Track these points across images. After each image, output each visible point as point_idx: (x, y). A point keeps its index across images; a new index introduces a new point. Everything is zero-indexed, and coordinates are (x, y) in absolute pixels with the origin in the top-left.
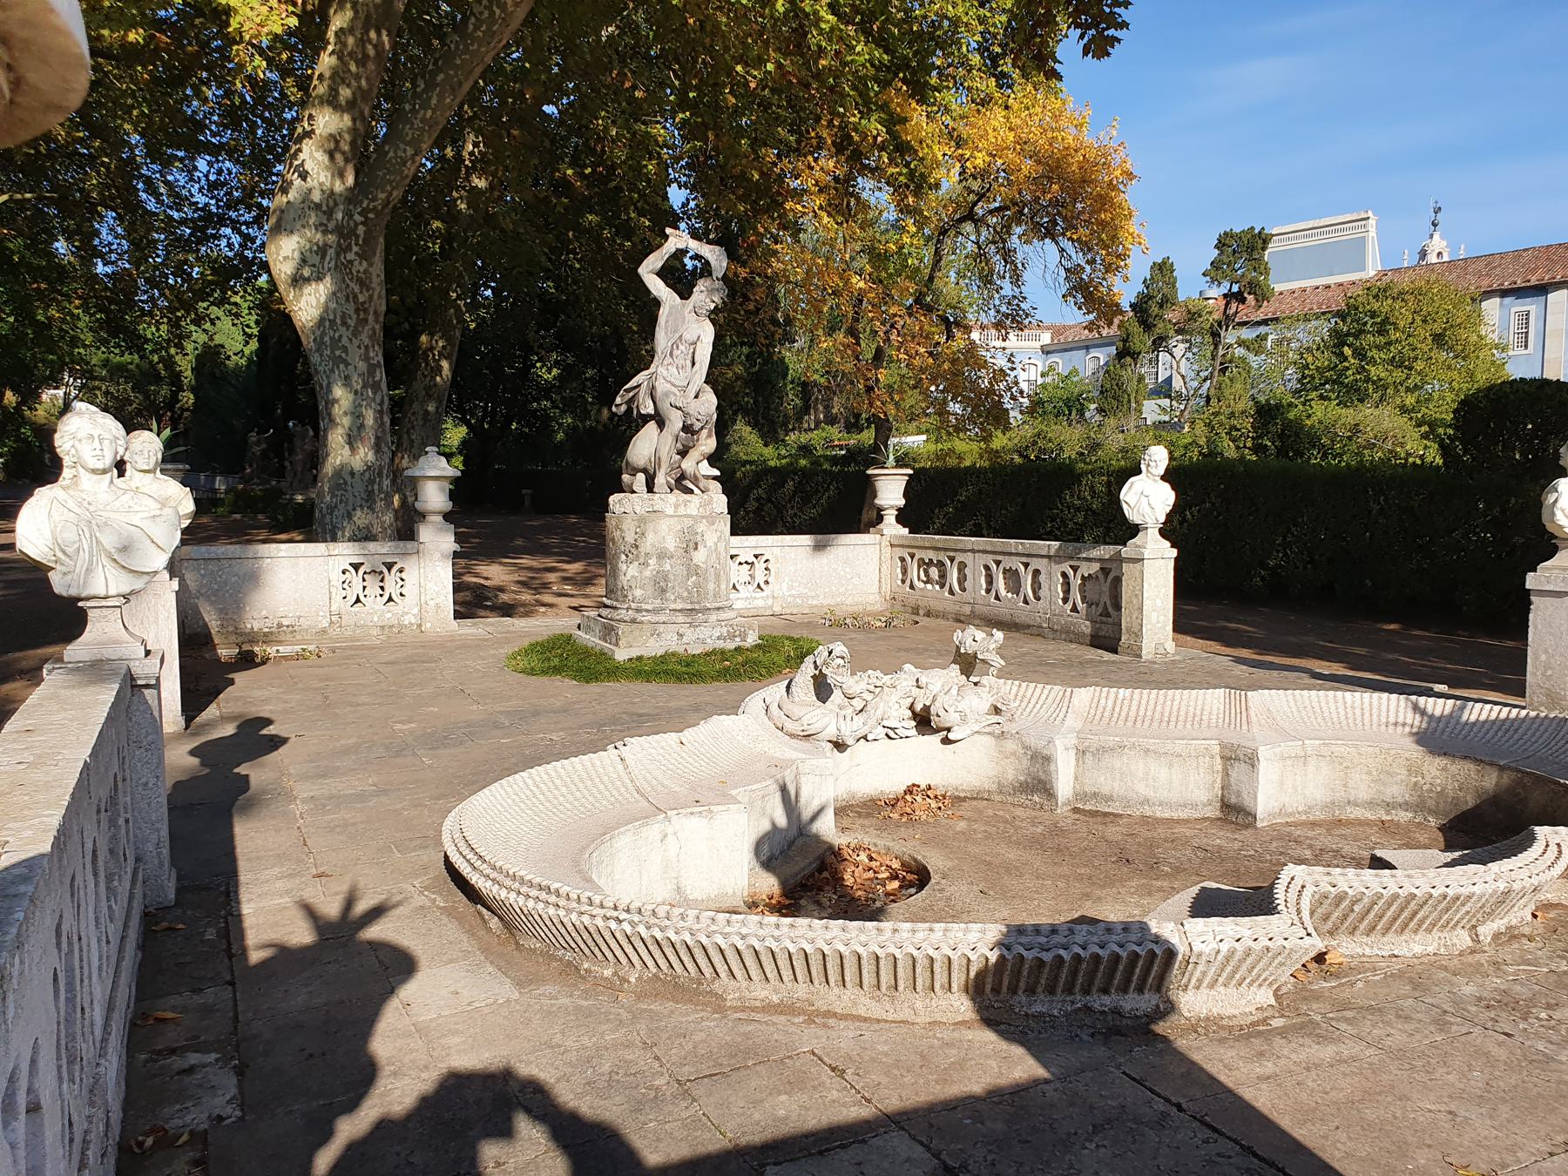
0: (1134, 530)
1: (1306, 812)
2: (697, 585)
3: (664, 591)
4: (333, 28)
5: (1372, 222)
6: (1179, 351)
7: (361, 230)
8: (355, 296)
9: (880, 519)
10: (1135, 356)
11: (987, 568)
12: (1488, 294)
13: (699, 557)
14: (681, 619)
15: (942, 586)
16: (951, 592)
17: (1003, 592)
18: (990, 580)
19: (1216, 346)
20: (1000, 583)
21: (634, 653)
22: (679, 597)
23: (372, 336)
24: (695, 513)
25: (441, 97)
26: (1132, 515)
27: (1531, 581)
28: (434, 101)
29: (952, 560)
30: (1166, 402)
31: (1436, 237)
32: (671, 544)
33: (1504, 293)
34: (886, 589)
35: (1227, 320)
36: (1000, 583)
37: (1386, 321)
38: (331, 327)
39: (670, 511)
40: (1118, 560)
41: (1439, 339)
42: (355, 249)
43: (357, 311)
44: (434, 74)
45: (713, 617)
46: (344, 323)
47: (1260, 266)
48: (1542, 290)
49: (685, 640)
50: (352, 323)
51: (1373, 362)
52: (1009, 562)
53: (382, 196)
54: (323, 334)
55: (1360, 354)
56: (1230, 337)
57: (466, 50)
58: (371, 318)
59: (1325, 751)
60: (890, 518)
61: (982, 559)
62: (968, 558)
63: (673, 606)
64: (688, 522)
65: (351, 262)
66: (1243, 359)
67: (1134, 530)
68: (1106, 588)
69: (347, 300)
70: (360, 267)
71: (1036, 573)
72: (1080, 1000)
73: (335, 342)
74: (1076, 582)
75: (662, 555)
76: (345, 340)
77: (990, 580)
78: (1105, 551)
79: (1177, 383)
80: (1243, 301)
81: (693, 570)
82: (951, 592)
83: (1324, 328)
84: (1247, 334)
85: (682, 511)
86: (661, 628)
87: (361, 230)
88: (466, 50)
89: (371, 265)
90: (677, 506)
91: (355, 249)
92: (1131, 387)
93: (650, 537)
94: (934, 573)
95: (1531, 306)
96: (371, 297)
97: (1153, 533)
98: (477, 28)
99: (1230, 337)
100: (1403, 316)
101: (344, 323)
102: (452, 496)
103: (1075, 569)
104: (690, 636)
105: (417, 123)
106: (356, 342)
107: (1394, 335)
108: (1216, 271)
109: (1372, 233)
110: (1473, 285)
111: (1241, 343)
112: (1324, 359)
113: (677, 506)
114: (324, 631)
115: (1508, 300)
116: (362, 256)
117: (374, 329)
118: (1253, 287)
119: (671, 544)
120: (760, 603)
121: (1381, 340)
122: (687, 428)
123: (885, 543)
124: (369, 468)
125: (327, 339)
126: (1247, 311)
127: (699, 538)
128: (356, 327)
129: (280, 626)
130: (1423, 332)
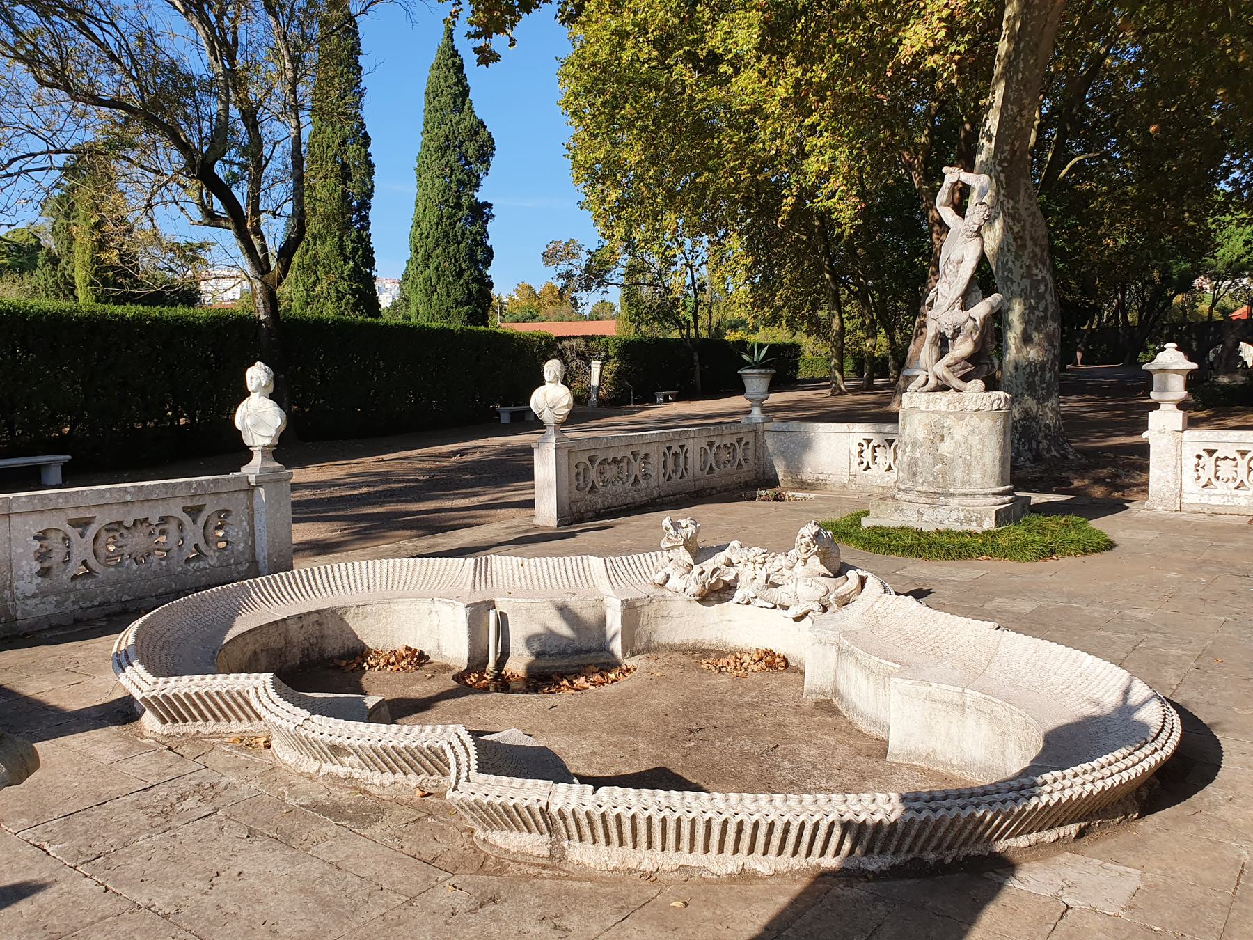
1: (961, 769)
3: (914, 474)
4: (1006, 16)
13: (945, 448)
14: (923, 499)
21: (877, 523)
22: (926, 481)
23: (1034, 257)
24: (944, 409)
25: (1026, 61)
28: (1021, 65)
32: (921, 435)
39: (923, 408)
43: (1015, 239)
45: (955, 502)
49: (925, 518)
50: (1013, 249)
53: (1007, 148)
58: (1029, 243)
59: (984, 706)
63: (919, 488)
64: (935, 417)
72: (684, 858)
75: (915, 445)
76: (1010, 263)
85: (932, 407)
86: (904, 505)
89: (1017, 202)
90: (928, 403)
96: (1023, 227)
102: (1188, 386)
104: (929, 515)
106: (1018, 264)
113: (928, 403)
114: (845, 486)
117: (1033, 251)
119: (921, 435)
120: (1236, 501)
124: (1030, 364)
127: (945, 431)
128: (1017, 253)
129: (818, 479)
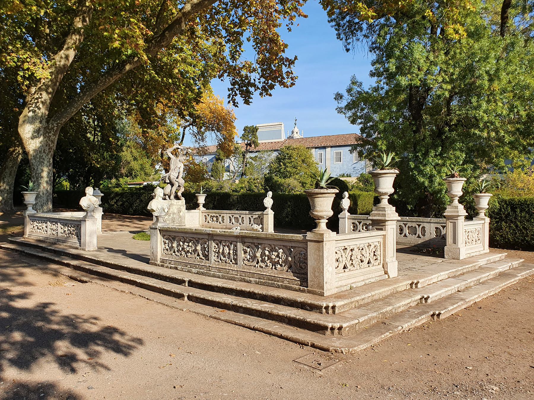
0: (266, 208)
2: (181, 220)
5: (283, 125)
6: (233, 159)
7: (55, 128)
8: (49, 145)
9: (199, 206)
10: (221, 160)
11: (230, 217)
12: (313, 148)
13: (181, 214)
15: (217, 222)
16: (220, 223)
17: (234, 222)
18: (230, 220)
19: (244, 158)
20: (233, 220)
26: (266, 205)
27: (339, 216)
29: (220, 216)
30: (228, 173)
31: (296, 127)
32: (176, 211)
33: (316, 148)
34: (201, 223)
35: (247, 151)
36: (233, 220)
37: (290, 156)
38: (40, 153)
40: (263, 214)
41: (303, 161)
42: (52, 133)
43: (49, 149)
44: (86, 92)
46: (44, 152)
47: (255, 136)
48: (325, 148)
50: (47, 152)
51: (287, 167)
52: (235, 216)
54: (37, 155)
55: (284, 164)
56: (248, 155)
57: (96, 88)
60: (201, 206)
61: (229, 215)
62: (225, 215)
65: (50, 136)
66: (251, 162)
67: (266, 208)
68: (259, 220)
69: (47, 146)
70: (52, 137)
71: (243, 218)
73: (41, 157)
74: (252, 220)
75: (174, 214)
76: (44, 157)
77: (230, 220)
78: (260, 213)
79: (232, 168)
80: (251, 146)
81: (180, 217)
82: (220, 223)
83: (275, 154)
84: (253, 155)
85: (178, 204)
87: (55, 128)
88: (96, 88)
91: (52, 133)
92: (221, 169)
93: (171, 209)
94: (215, 219)
95: (322, 151)
97: (270, 209)
98: (100, 83)
99: (248, 155)
100: (295, 155)
101: (44, 152)
103: (252, 217)
105: (79, 103)
107: (293, 160)
108: (244, 137)
109: (283, 129)
110: (308, 145)
111: (251, 158)
112: (276, 165)
115: (317, 150)
116: (54, 135)
118: (254, 142)
119: (176, 211)
121: (289, 161)
122: (179, 186)
123: (201, 212)
125: (38, 156)
126: (252, 148)
130: (300, 159)
